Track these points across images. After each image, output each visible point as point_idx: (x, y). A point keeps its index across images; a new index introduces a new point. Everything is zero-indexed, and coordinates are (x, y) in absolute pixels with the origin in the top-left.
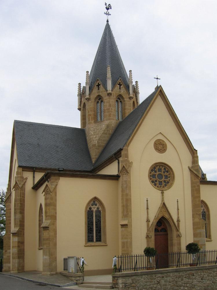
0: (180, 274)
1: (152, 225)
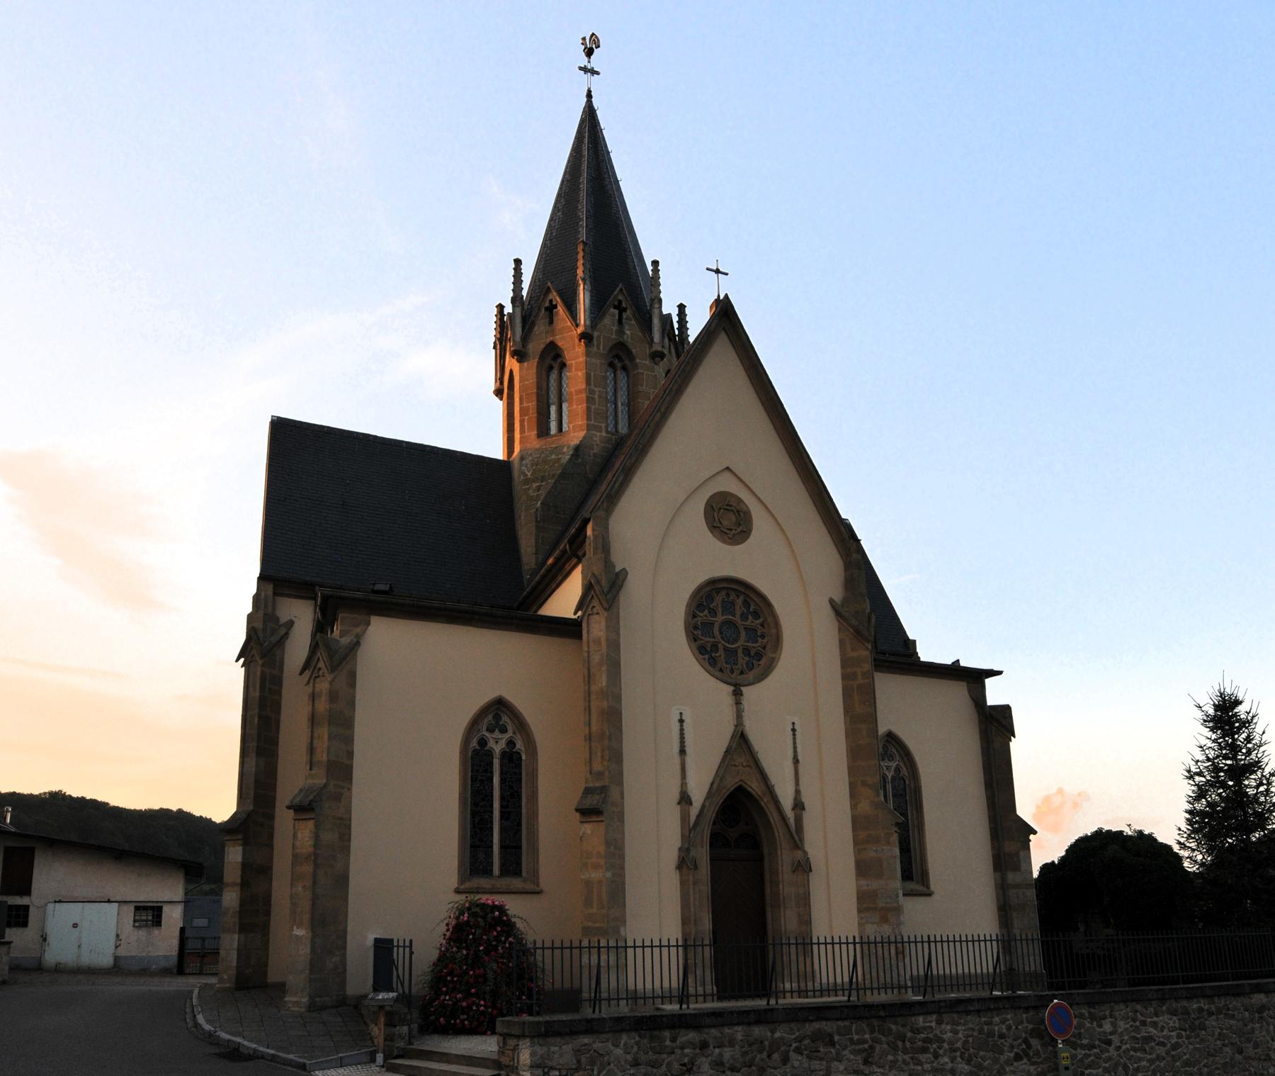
0: (777, 1035)
1: (698, 816)
